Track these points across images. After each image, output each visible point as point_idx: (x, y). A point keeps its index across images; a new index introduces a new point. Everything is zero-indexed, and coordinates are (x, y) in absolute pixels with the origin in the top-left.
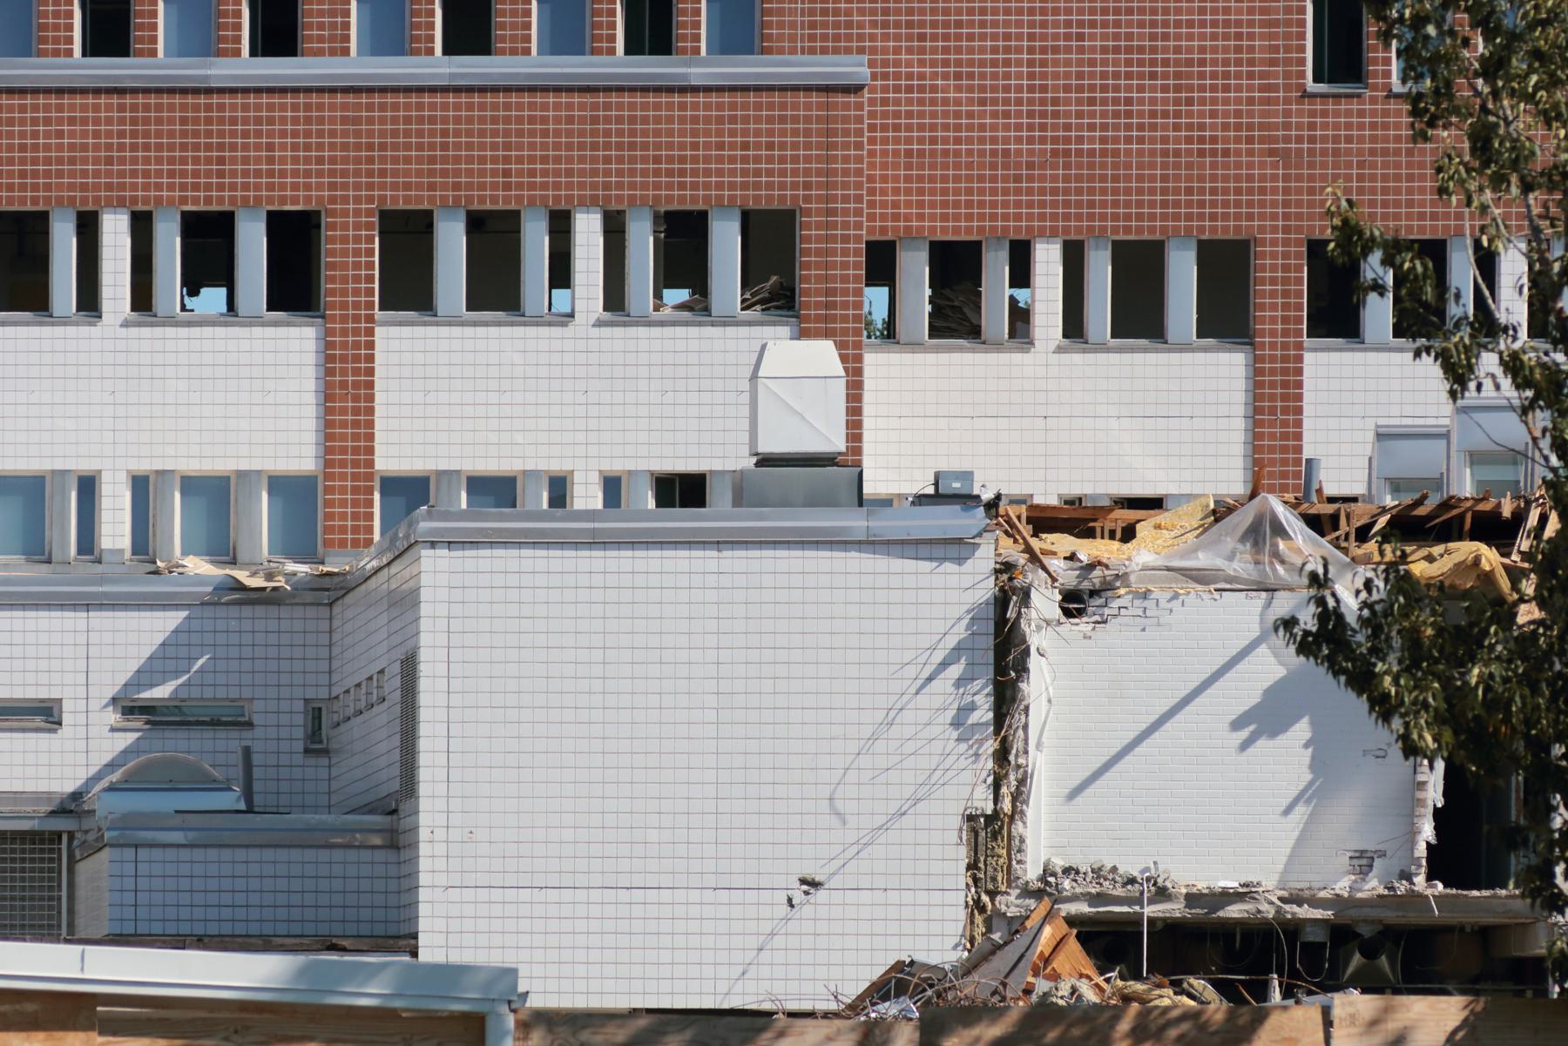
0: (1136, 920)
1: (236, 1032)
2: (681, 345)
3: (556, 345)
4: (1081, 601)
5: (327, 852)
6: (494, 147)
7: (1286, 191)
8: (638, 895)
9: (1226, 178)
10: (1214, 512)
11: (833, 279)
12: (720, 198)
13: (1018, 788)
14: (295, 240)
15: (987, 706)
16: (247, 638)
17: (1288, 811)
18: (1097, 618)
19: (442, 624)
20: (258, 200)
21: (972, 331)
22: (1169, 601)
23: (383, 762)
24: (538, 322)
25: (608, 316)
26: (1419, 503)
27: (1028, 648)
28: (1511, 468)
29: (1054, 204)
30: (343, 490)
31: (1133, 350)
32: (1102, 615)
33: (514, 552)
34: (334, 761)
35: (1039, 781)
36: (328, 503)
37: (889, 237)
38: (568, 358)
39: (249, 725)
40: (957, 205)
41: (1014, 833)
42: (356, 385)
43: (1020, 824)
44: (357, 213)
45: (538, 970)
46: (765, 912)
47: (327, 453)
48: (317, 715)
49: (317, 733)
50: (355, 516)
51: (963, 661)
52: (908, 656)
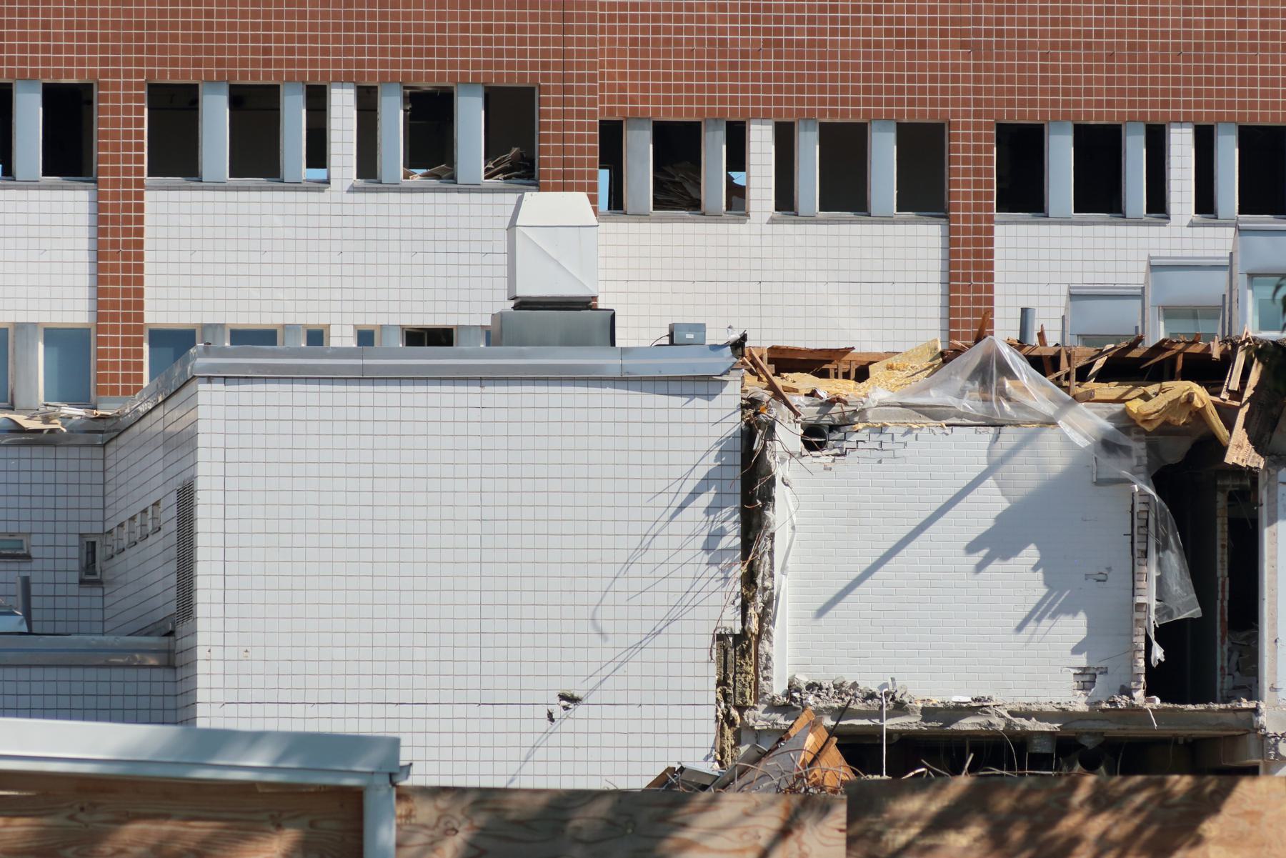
0: (875, 733)
1: (82, 809)
4: (821, 435)
5: (107, 671)
6: (255, 26)
7: (977, 79)
9: (922, 68)
10: (942, 354)
11: (570, 150)
12: (464, 76)
13: (764, 609)
14: (174, 112)
15: (735, 532)
16: (25, 477)
17: (1019, 628)
19: (218, 455)
20: (34, 74)
21: (693, 204)
23: (158, 588)
24: (297, 187)
26: (1133, 346)
28: (1191, 322)
29: (767, 89)
30: (114, 342)
31: (839, 222)
32: (841, 448)
34: (107, 591)
36: (101, 354)
37: (617, 117)
38: (325, 221)
39: (27, 557)
40: (678, 89)
41: (761, 651)
44: (128, 86)
47: (98, 307)
49: (92, 565)
51: (713, 490)
52: (661, 485)
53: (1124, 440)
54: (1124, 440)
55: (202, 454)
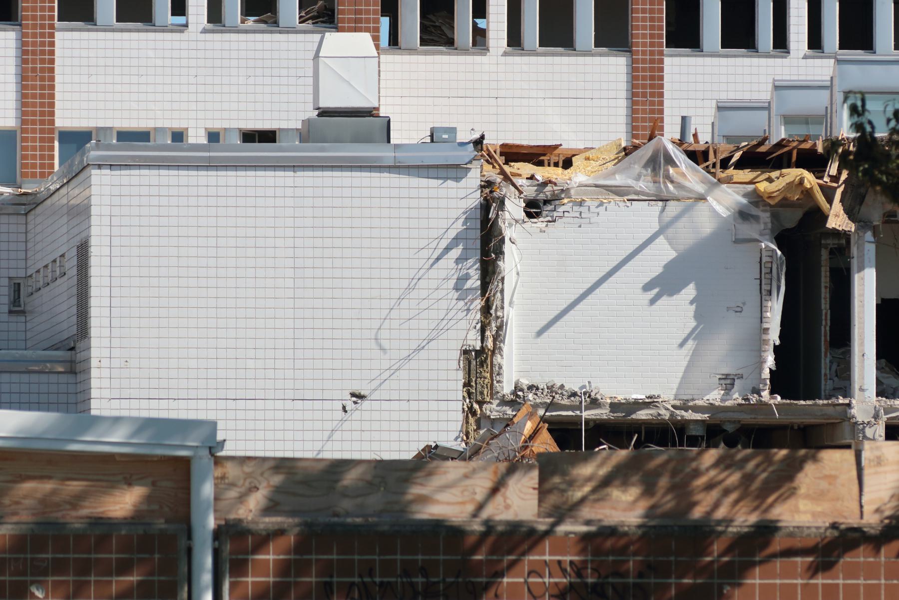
0: (576, 421)
2: (259, 46)
3: (176, 45)
4: (538, 207)
8: (241, 404)
10: (625, 149)
17: (682, 345)
18: (549, 218)
19: (106, 221)
21: (449, 42)
22: (597, 207)
23: (64, 316)
24: (164, 29)
25: (211, 26)
26: (761, 143)
27: (504, 238)
28: (804, 126)
31: (553, 55)
32: (552, 217)
33: (155, 172)
34: (28, 319)
35: (511, 328)
36: (24, 148)
41: (495, 362)
42: (42, 70)
43: (499, 356)
45: (231, 425)
46: (327, 415)
48: (17, 288)
50: (42, 157)
51: (461, 247)
53: (754, 211)
54: (754, 211)
55: (94, 220)
